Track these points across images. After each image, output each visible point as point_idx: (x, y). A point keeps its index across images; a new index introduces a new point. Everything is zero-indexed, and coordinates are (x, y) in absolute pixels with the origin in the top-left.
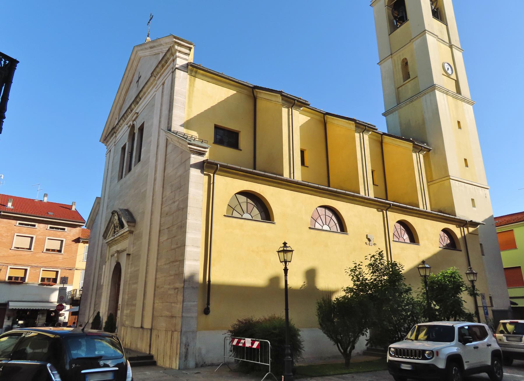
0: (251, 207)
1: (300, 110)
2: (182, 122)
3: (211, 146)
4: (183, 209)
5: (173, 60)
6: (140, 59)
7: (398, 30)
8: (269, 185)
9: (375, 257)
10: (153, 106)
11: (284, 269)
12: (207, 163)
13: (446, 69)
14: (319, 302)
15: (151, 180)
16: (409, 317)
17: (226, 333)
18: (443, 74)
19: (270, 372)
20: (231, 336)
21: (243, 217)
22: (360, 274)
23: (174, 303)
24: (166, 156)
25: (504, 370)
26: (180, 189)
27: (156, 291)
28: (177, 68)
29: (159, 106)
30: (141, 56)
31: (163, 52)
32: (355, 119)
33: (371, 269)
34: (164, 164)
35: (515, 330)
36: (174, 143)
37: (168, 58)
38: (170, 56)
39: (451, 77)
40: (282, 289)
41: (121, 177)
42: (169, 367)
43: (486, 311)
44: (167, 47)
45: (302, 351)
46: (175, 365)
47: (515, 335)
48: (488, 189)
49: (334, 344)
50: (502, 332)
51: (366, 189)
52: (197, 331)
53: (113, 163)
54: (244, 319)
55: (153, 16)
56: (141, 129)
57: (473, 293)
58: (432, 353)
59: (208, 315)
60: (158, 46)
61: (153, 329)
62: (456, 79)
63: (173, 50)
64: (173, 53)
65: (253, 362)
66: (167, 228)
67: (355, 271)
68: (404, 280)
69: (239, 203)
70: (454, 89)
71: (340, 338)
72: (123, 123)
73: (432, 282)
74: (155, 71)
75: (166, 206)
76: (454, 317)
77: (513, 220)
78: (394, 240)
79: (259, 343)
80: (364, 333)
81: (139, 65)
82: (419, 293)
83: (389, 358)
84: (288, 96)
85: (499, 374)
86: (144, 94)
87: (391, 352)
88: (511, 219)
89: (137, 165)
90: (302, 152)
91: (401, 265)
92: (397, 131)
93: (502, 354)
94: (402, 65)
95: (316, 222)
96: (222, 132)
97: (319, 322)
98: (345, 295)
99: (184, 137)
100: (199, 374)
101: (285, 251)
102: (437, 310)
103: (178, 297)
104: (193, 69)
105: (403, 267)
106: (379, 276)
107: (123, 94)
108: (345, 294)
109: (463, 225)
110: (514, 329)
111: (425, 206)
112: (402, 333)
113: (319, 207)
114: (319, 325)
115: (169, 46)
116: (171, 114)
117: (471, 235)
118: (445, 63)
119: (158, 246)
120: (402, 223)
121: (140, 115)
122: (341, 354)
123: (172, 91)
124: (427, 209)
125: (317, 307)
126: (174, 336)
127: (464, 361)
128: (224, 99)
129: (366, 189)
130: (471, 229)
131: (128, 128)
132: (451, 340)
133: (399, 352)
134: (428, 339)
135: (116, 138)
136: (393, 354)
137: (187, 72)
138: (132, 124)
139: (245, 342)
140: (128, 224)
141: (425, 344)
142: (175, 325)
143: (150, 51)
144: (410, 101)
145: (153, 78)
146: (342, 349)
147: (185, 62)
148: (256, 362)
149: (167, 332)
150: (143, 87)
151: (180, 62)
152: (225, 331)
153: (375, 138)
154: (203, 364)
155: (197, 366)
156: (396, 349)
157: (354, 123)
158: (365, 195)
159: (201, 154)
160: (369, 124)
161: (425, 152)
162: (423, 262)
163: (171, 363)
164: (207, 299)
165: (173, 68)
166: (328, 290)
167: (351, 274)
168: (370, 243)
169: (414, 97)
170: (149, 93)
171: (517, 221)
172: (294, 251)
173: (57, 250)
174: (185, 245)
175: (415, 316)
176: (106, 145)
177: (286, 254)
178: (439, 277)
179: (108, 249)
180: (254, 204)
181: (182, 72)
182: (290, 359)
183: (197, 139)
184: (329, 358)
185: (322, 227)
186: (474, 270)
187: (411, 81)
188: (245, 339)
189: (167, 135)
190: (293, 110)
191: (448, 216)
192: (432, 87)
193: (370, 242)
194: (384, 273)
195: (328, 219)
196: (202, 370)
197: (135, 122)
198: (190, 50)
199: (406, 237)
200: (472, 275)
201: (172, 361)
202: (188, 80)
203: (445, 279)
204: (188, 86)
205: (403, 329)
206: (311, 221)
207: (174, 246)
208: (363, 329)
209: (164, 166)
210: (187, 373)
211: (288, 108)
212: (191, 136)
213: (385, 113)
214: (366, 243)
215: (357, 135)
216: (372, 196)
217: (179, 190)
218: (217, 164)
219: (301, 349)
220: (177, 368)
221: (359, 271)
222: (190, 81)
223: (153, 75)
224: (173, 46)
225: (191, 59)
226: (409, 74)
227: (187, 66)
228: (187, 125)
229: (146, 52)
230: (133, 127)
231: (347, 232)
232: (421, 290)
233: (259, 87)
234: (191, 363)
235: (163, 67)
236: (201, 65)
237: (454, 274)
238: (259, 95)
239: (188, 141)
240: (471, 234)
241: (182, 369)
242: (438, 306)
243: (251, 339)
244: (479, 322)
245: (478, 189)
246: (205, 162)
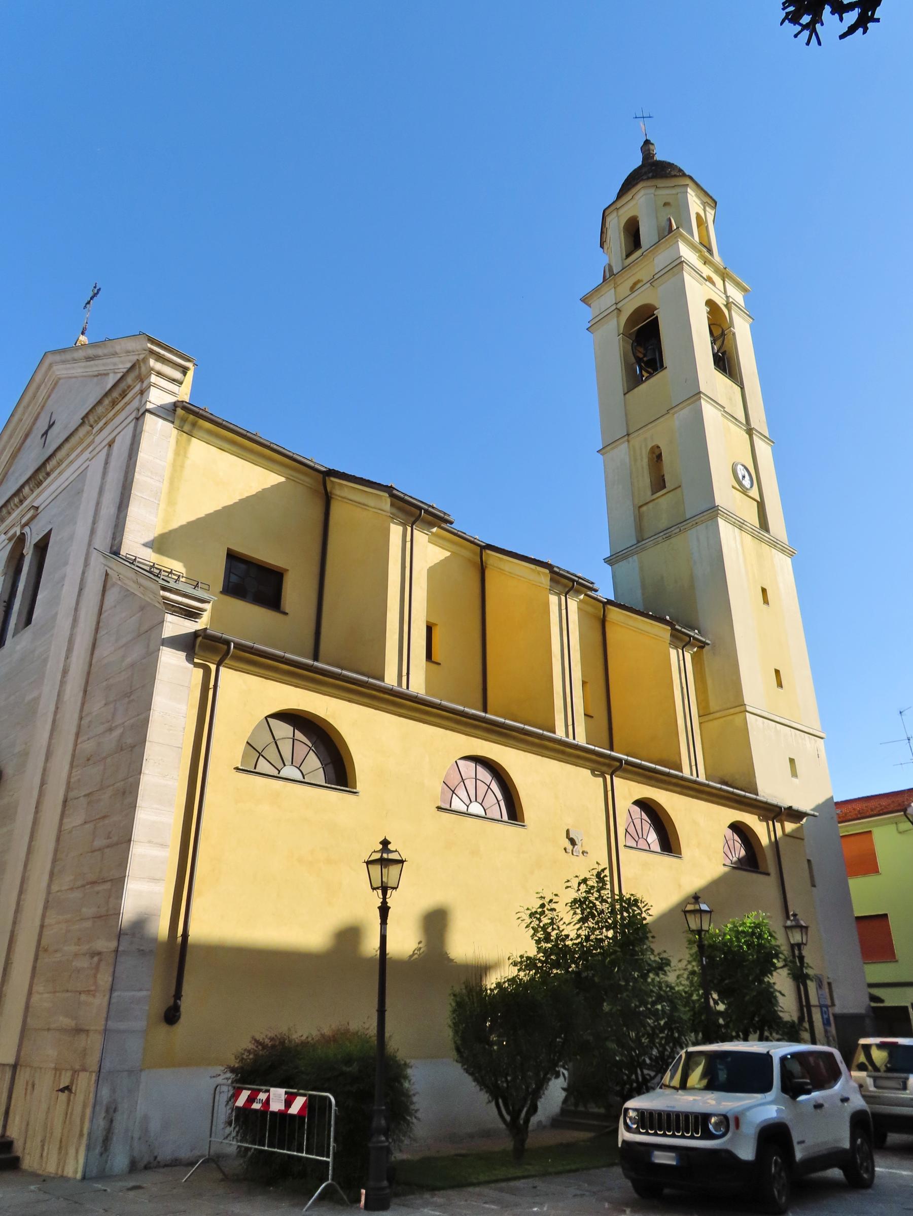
0: (301, 750)
1: (431, 532)
2: (150, 537)
3: (216, 598)
4: (133, 747)
5: (142, 391)
6: (56, 384)
7: (643, 387)
8: (349, 701)
9: (588, 882)
10: (79, 493)
11: (378, 908)
12: (203, 638)
13: (741, 477)
14: (457, 991)
15: (54, 668)
16: (662, 1030)
17: (219, 1072)
18: (734, 485)
19: (330, 1181)
20: (232, 1083)
21: (282, 774)
22: (552, 923)
23: (88, 992)
24: (100, 613)
25: (877, 1159)
26: (129, 697)
27: (39, 961)
29: (95, 494)
30: (58, 376)
31: (116, 371)
32: (551, 565)
33: (578, 911)
34: (93, 635)
35: (889, 1062)
36: (125, 584)
37: (129, 387)
38: (134, 381)
39: (750, 494)
40: (371, 960)
42: (57, 1174)
43: (825, 1016)
44: (130, 361)
45: (414, 1120)
46: (74, 1167)
47: (890, 1075)
48: (822, 738)
49: (489, 1102)
50: (862, 1067)
51: (570, 722)
52: (141, 1070)
54: (269, 1037)
55: (99, 290)
56: (42, 547)
57: (800, 977)
58: (728, 1122)
59: (176, 1025)
60: (105, 355)
61: (21, 1066)
62: (759, 500)
63: (143, 369)
64: (143, 376)
65: (286, 1154)
66: (85, 796)
67: (540, 916)
68: (650, 939)
69: (274, 739)
70: (753, 518)
71: (505, 1085)
73: (713, 947)
74: (93, 412)
75: (88, 739)
76: (758, 1031)
77: (872, 810)
78: (627, 845)
79: (306, 1100)
80: (559, 1071)
81: (53, 396)
82: (682, 972)
83: (624, 1135)
84: (406, 498)
85: (867, 1171)
87: (628, 1121)
88: (866, 807)
89: (19, 635)
90: (429, 629)
91: (645, 903)
92: (636, 599)
93: (872, 1124)
94: (650, 460)
95: (454, 795)
96: (243, 566)
97: (455, 1042)
98: (517, 976)
99: (153, 572)
100: (141, 1191)
101: (384, 863)
102: (720, 1013)
103: (99, 976)
104: (188, 418)
105: (649, 909)
106: (593, 930)
108: (516, 973)
109: (773, 815)
110: (887, 1060)
111: (694, 768)
112: (646, 1072)
113: (461, 758)
114: (455, 1053)
115: (134, 358)
116: (122, 515)
117: (788, 838)
118: (737, 465)
119: (58, 839)
120: (644, 805)
121: (42, 513)
122: (502, 1126)
123: (133, 460)
124: (698, 776)
125: (450, 1004)
126: (77, 1084)
127: (796, 1137)
128: (254, 493)
129: (569, 724)
130: (790, 827)
131: (7, 541)
132: (765, 1088)
133: (648, 1120)
134: (712, 1086)
136: (634, 1124)
137: (173, 422)
138: (18, 533)
139: (268, 1099)
141: (708, 1099)
142: (84, 1053)
143: (85, 367)
144: (664, 537)
145: (86, 428)
146: (508, 1113)
147: (170, 399)
148: (295, 1153)
149: (60, 1074)
150: (59, 448)
151: (157, 397)
152: (219, 1069)
153: (590, 609)
154: (149, 1163)
155: (134, 1167)
156: (641, 1113)
157: (547, 571)
158: (567, 736)
159: (191, 614)
160: (579, 578)
161: (695, 649)
162: (696, 898)
163: (62, 1162)
164: (174, 981)
165: (139, 410)
166: (485, 961)
167: (531, 923)
168: (574, 850)
169: (673, 529)
170: (72, 462)
171: (879, 811)
172: (405, 861)
174: (130, 840)
175: (677, 1028)
177: (387, 869)
178: (725, 934)
180: (311, 745)
181: (160, 421)
182: (382, 1142)
183: (183, 580)
184: (471, 1136)
185: (468, 807)
186: (802, 919)
187: (667, 495)
188: (268, 1091)
189: (109, 564)
190: (415, 531)
191: (743, 793)
192: (712, 511)
193: (574, 847)
194: (607, 921)
195: (482, 788)
196: (149, 1180)
197: (27, 530)
198: (185, 374)
199: (653, 837)
200: (798, 930)
201: (67, 1154)
202: (173, 441)
203: (738, 940)
204: (170, 455)
205: (648, 1061)
206: (443, 792)
207: (98, 843)
208: (559, 1060)
209: (91, 640)
210: (105, 1190)
211: (404, 525)
212: (170, 571)
213: (611, 558)
214: (565, 849)
215: (553, 599)
216: (581, 739)
217: (127, 700)
218: (227, 643)
219: (410, 1115)
220: (79, 1176)
221: (550, 916)
222: (177, 442)
223: (87, 422)
224: (145, 360)
225: (184, 393)
226: (664, 481)
227: (173, 408)
228: (160, 544)
229: (73, 368)
230: (21, 540)
231: (524, 822)
232: (686, 966)
233: (340, 472)
234: (119, 1160)
235: (113, 405)
236: (207, 410)
237: (759, 928)
238: (337, 492)
239: (161, 582)
240: (792, 839)
241: (91, 1179)
242: (723, 1003)
243: (284, 1090)
244: (814, 1042)
245: (803, 737)
246: (200, 636)
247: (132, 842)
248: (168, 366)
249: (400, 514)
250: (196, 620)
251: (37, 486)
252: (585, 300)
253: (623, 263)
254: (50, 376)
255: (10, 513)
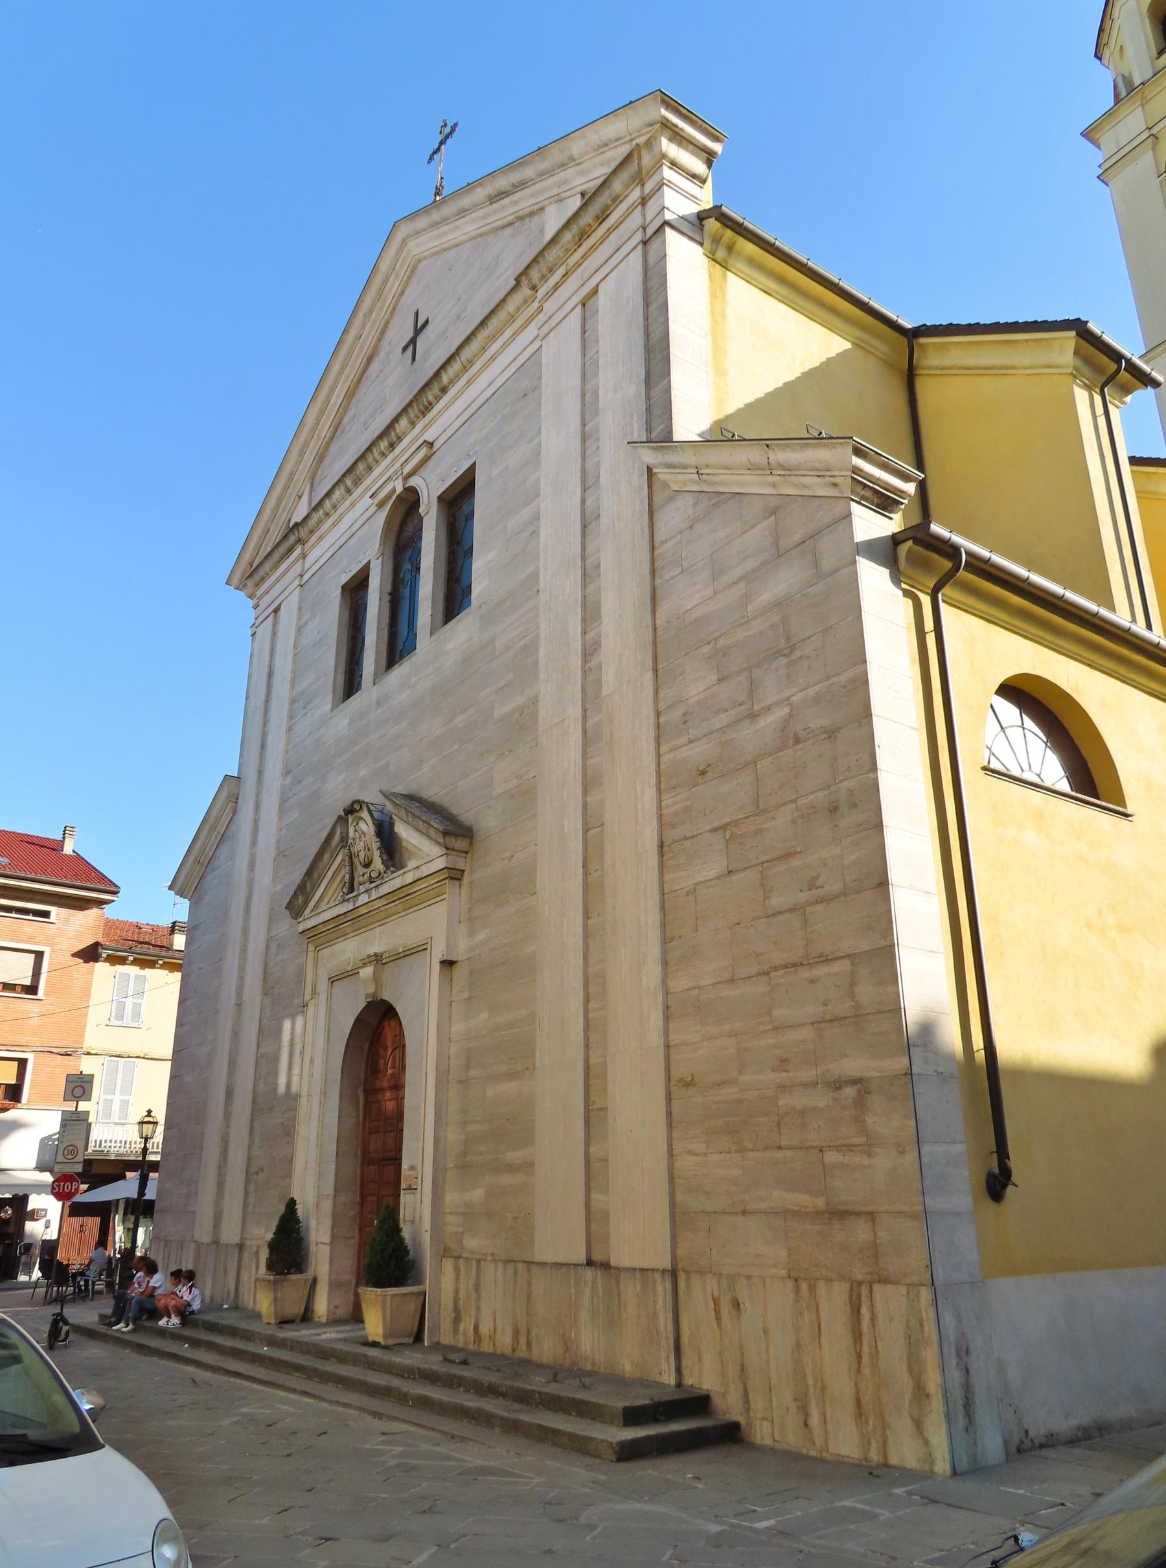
5: (643, 199)
6: (412, 271)
8: (1090, 666)
28: (666, 223)
30: (416, 257)
38: (627, 186)
41: (351, 684)
53: (295, 647)
72: (344, 499)
86: (465, 367)
107: (335, 403)
119: (663, 908)
128: (818, 364)
135: (304, 563)
137: (701, 244)
140: (448, 839)
165: (644, 229)
170: (493, 358)
173: (23, 986)
176: (251, 597)
179: (311, 955)
222: (710, 276)
224: (650, 143)
234: (992, 1445)
235: (580, 239)
247: (890, 886)
248: (686, 149)
249: (1086, 370)
250: (891, 515)
251: (423, 413)
252: (1089, 134)
253: (1153, 66)
254: (403, 260)
255: (377, 462)
